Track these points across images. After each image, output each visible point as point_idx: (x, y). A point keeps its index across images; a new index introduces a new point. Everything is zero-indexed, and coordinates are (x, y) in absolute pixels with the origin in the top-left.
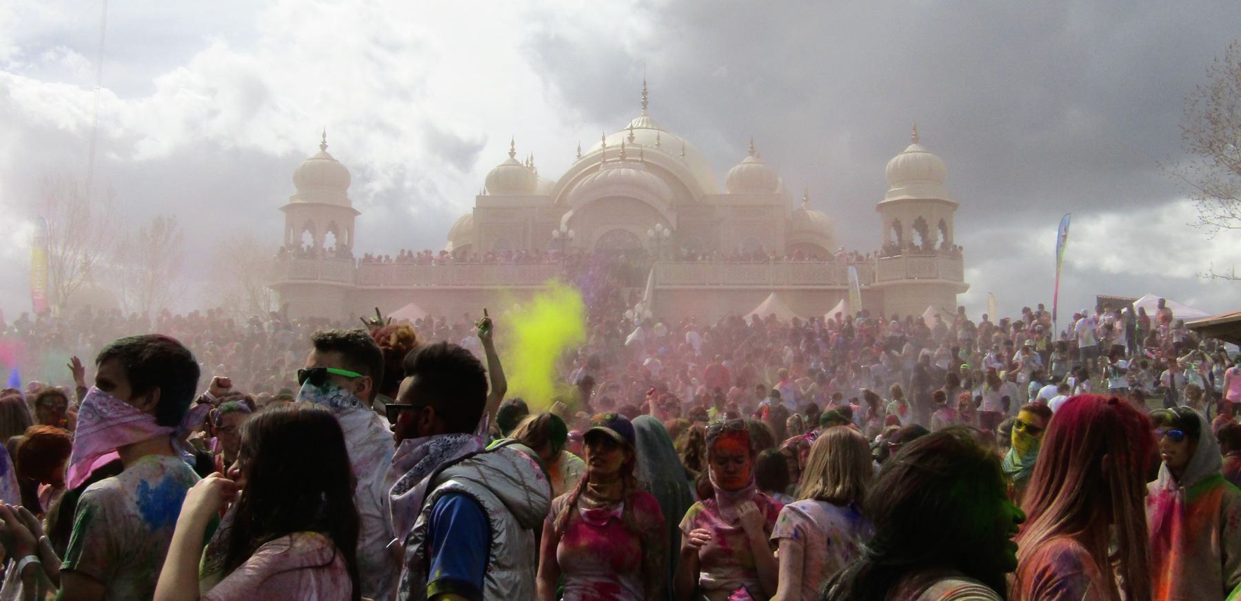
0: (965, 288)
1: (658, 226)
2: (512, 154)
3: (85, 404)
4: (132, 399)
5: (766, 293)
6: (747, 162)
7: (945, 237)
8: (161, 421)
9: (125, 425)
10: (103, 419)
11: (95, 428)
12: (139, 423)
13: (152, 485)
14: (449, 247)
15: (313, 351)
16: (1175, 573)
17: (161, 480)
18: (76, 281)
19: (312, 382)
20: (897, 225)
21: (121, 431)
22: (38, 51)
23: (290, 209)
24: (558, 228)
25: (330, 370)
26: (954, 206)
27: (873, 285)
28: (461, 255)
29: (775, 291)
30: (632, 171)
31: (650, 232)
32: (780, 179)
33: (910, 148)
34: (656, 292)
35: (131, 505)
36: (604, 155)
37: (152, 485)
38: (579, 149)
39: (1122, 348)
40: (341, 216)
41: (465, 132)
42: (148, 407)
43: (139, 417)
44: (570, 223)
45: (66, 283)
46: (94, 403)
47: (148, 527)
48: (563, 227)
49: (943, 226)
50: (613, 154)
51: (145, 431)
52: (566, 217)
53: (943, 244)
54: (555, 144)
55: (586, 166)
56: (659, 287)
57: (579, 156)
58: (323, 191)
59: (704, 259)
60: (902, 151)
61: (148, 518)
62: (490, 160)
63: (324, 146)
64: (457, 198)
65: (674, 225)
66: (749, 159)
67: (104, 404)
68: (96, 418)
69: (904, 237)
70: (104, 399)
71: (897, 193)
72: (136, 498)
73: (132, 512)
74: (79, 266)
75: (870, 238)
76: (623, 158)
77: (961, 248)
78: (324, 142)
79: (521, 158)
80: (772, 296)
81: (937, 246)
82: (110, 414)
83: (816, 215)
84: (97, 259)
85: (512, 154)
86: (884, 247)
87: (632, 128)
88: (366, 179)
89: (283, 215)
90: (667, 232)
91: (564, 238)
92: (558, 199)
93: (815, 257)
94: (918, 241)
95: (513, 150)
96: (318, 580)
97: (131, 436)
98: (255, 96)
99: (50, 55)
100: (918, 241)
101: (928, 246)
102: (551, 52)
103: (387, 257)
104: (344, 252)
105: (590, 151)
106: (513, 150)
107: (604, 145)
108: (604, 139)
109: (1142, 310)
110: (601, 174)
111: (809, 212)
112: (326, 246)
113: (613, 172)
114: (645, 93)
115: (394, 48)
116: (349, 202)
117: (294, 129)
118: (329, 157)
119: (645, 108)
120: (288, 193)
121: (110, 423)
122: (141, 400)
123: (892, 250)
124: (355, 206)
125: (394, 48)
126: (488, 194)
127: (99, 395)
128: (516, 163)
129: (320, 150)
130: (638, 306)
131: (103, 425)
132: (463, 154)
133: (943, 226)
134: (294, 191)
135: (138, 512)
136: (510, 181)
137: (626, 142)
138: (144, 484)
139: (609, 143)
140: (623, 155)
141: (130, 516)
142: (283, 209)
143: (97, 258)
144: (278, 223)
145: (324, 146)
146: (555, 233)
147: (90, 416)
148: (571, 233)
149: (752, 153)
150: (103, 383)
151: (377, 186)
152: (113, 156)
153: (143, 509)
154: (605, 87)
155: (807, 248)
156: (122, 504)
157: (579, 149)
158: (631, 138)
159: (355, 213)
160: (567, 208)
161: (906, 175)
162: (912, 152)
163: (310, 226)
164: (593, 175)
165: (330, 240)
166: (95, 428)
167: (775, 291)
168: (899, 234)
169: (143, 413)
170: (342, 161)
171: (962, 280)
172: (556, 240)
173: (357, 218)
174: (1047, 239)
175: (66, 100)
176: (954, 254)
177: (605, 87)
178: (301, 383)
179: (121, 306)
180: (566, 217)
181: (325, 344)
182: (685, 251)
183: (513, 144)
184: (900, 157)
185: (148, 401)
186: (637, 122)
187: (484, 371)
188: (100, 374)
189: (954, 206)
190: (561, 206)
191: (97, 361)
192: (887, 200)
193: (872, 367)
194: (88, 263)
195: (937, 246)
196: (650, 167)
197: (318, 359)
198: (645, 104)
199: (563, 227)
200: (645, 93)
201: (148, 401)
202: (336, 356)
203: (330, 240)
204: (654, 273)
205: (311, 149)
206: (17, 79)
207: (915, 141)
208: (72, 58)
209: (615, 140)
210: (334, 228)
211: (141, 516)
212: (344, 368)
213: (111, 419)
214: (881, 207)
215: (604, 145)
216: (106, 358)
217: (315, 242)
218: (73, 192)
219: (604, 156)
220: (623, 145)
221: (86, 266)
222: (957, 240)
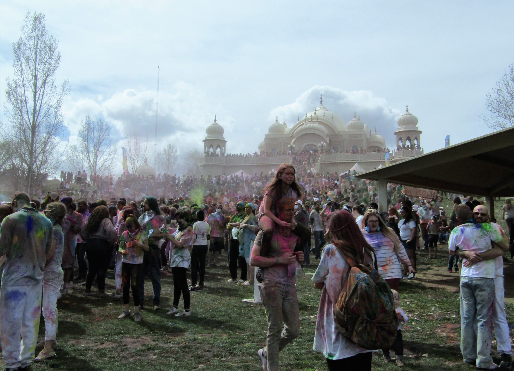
2: (277, 120)
16: (259, 243)
23: (205, 141)
31: (319, 145)
36: (305, 120)
44: (294, 143)
50: (308, 119)
65: (328, 141)
76: (312, 121)
79: (281, 122)
80: (356, 164)
85: (277, 120)
96: (294, 258)
101: (412, 147)
110: (303, 127)
113: (308, 125)
129: (405, 112)
134: (206, 135)
142: (396, 133)
144: (202, 144)
148: (294, 146)
167: (358, 163)
180: (293, 140)
196: (321, 123)
200: (321, 98)
203: (401, 144)
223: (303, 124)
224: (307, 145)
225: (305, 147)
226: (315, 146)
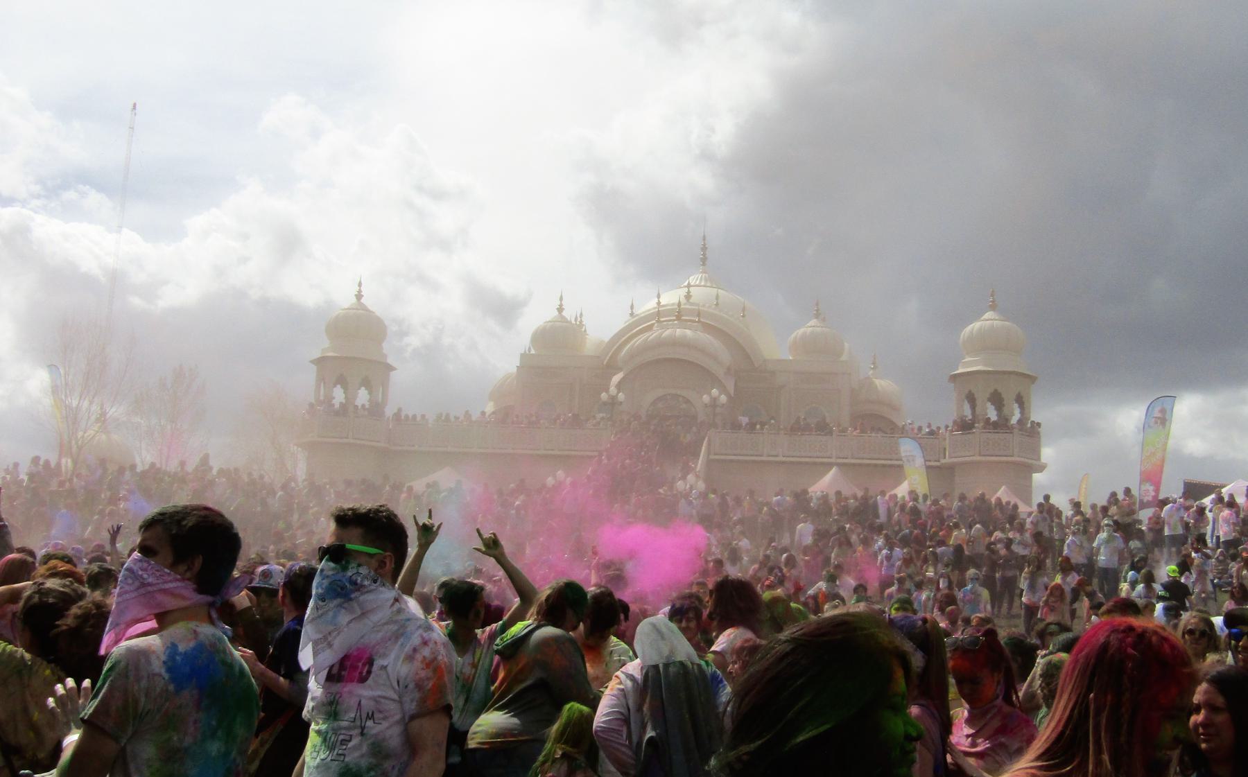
0: (1041, 468)
1: (715, 392)
2: (560, 309)
3: (127, 569)
4: (173, 566)
5: (830, 465)
6: (811, 326)
7: (1022, 413)
8: (201, 590)
9: (165, 591)
10: (143, 585)
11: (135, 594)
12: (178, 589)
13: (182, 648)
14: (490, 408)
15: (333, 525)
17: (192, 644)
18: (91, 432)
19: (331, 559)
20: (971, 399)
21: (160, 597)
22: (59, 187)
23: (320, 362)
24: (607, 390)
25: (349, 546)
26: (1032, 379)
27: (943, 461)
28: (504, 416)
29: (838, 465)
30: (688, 332)
31: (706, 398)
32: (846, 345)
33: (987, 316)
34: (709, 463)
35: (157, 666)
36: (658, 314)
37: (182, 648)
38: (632, 307)
39: (277, 591)
40: (375, 372)
41: (508, 286)
42: (188, 575)
43: (179, 584)
45: (80, 434)
46: (135, 568)
47: (171, 687)
48: (613, 390)
49: (1020, 400)
50: (668, 313)
51: (184, 598)
52: (616, 379)
53: (1020, 421)
54: (608, 303)
55: (638, 325)
56: (712, 457)
57: (632, 314)
58: (355, 347)
59: (762, 428)
60: (978, 316)
61: (173, 680)
62: (536, 316)
63: (359, 296)
64: (501, 356)
65: (732, 392)
66: (813, 322)
67: (145, 570)
68: (137, 584)
69: (978, 410)
70: (145, 565)
71: (970, 364)
72: (163, 658)
73: (157, 670)
74: (93, 418)
75: (944, 410)
76: (679, 318)
77: (1039, 425)
78: (360, 291)
79: (569, 314)
80: (834, 470)
81: (1014, 420)
82: (150, 580)
83: (883, 384)
84: (113, 411)
85: (560, 309)
86: (955, 422)
87: (689, 286)
88: (403, 334)
89: (314, 368)
90: (723, 398)
91: (613, 402)
92: (606, 364)
93: (879, 429)
94: (993, 415)
95: (561, 305)
97: (171, 603)
98: (288, 244)
99: (71, 195)
100: (993, 415)
102: (605, 205)
103: (423, 416)
104: (376, 410)
105: (643, 309)
106: (561, 305)
107: (659, 303)
108: (659, 296)
109: (1231, 496)
110: (652, 335)
111: (877, 382)
112: (359, 402)
113: (668, 332)
114: (704, 248)
115: (438, 195)
116: (385, 356)
117: (328, 280)
118: (365, 308)
119: (704, 264)
120: (321, 346)
121: (150, 589)
122: (182, 568)
123: (965, 426)
124: (390, 361)
125: (438, 195)
126: (533, 352)
127: (140, 561)
128: (563, 319)
129: (354, 300)
130: (691, 477)
131: (142, 591)
132: (504, 310)
133: (1020, 400)
134: (326, 343)
135: (163, 671)
136: (558, 337)
137: (683, 300)
138: (174, 646)
139: (663, 302)
140: (679, 314)
141: (154, 675)
143: (113, 410)
145: (359, 296)
146: (604, 396)
147: (130, 581)
148: (621, 396)
149: (817, 316)
150: (145, 549)
151: (414, 341)
152: (136, 301)
153: (169, 670)
154: (655, 242)
155: (876, 420)
156: (149, 662)
157: (632, 307)
158: (688, 296)
159: (390, 368)
160: (620, 369)
161: (983, 344)
162: (989, 320)
163: (341, 381)
164: (645, 335)
165: (363, 397)
166: (135, 594)
167: (838, 465)
168: (973, 407)
169: (183, 580)
170: (378, 314)
171: (1039, 459)
172: (605, 404)
173: (393, 374)
174: (1127, 418)
175: (91, 241)
176: (1032, 432)
177: (655, 242)
178: (321, 560)
179: (138, 460)
180: (616, 379)
181: (345, 520)
182: (744, 420)
183: (561, 299)
184: (976, 325)
185: (189, 569)
186: (694, 279)
187: (11, 654)
188: (142, 541)
189: (1032, 379)
190: (611, 368)
191: (141, 527)
192: (961, 370)
193: (939, 550)
194: (103, 414)
195: (1014, 420)
196: (708, 328)
197: (338, 535)
198: (704, 260)
199: (613, 390)
200: (704, 248)
201: (189, 569)
202: (356, 532)
203: (363, 397)
204: (709, 444)
205: (344, 299)
206: (40, 218)
207: (993, 307)
208: (94, 198)
209: (671, 298)
210: (366, 383)
211: (167, 676)
212: (364, 544)
213: (150, 585)
214: (954, 378)
215: (659, 303)
216: (150, 525)
217: (346, 398)
218: (86, 337)
219: (658, 314)
220: (679, 304)
221: (102, 418)
222: (1035, 416)
223: (650, 328)
224: (659, 399)
225: (654, 403)
226: (687, 401)
